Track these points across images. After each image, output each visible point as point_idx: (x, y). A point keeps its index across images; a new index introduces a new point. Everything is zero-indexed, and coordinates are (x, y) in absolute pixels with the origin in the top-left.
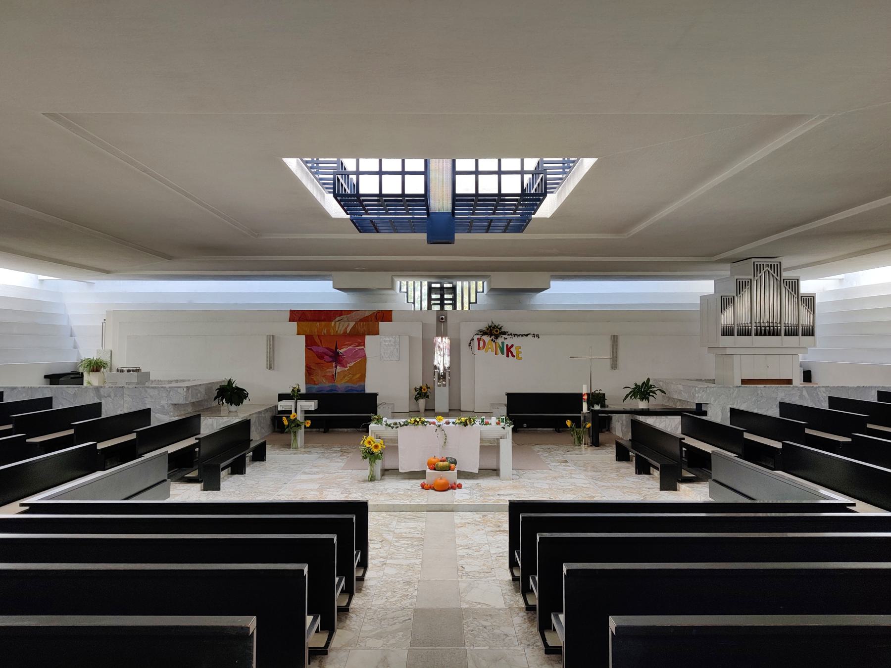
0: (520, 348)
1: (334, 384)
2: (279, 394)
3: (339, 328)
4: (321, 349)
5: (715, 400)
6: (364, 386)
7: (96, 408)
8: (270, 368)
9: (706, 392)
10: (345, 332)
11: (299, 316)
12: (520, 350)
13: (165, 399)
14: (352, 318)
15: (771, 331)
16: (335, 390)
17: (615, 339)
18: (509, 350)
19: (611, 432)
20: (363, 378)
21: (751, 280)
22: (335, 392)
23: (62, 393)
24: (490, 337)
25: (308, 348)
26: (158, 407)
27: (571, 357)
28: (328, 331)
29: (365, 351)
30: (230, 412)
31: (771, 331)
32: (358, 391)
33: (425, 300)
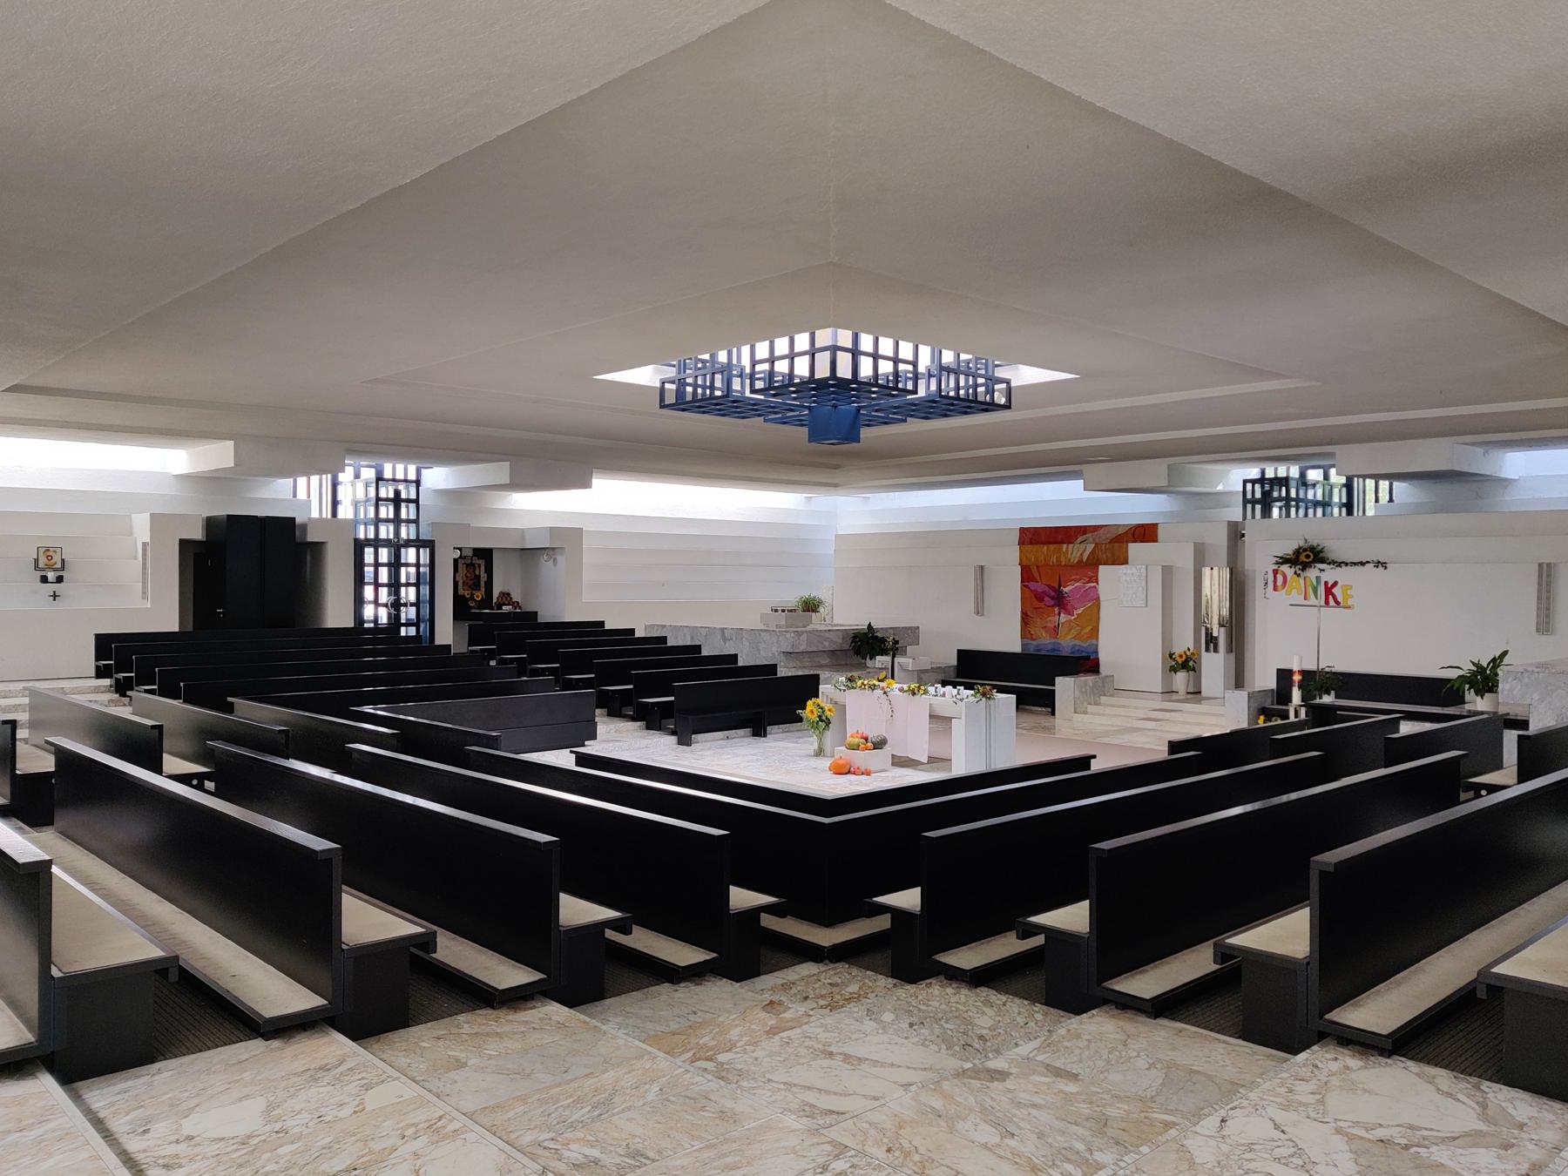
0: (1351, 587)
2: (959, 651)
3: (1071, 554)
5: (1541, 700)
6: (1097, 645)
7: (698, 648)
9: (1520, 681)
10: (1080, 561)
16: (1058, 650)
17: (1546, 573)
18: (1329, 591)
27: (1291, 605)
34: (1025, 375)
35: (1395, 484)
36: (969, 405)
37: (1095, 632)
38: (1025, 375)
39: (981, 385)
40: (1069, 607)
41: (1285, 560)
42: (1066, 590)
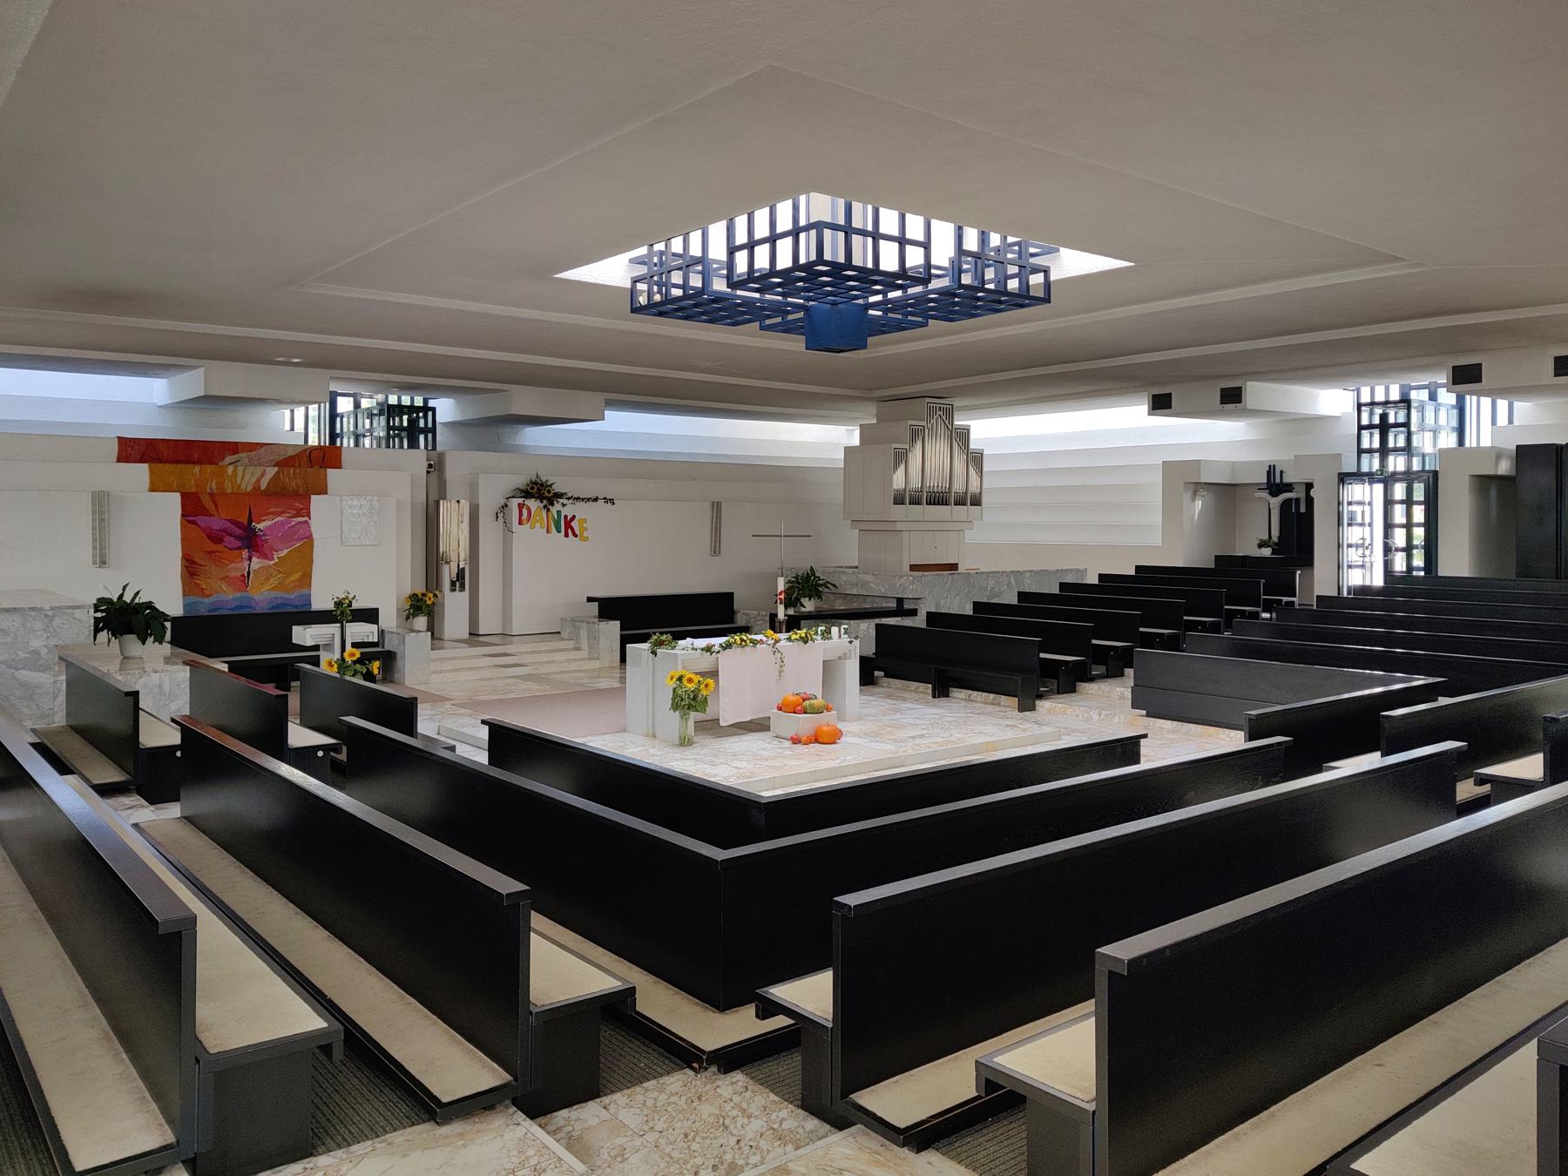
1: (245, 594)
3: (243, 478)
4: (216, 523)
8: (103, 563)
10: (257, 488)
11: (132, 450)
12: (585, 525)
13: (41, 635)
14: (259, 459)
15: (936, 500)
16: (250, 607)
17: (717, 508)
19: (399, 684)
20: (306, 579)
21: (924, 427)
22: (248, 611)
24: (542, 502)
25: (189, 521)
26: (22, 655)
28: (220, 484)
29: (309, 527)
30: (125, 658)
31: (936, 500)
32: (296, 607)
34: (1071, 263)
35: (1517, 405)
36: (1001, 301)
38: (1071, 263)
39: (1013, 276)
40: (266, 548)
41: (527, 493)
42: (261, 526)
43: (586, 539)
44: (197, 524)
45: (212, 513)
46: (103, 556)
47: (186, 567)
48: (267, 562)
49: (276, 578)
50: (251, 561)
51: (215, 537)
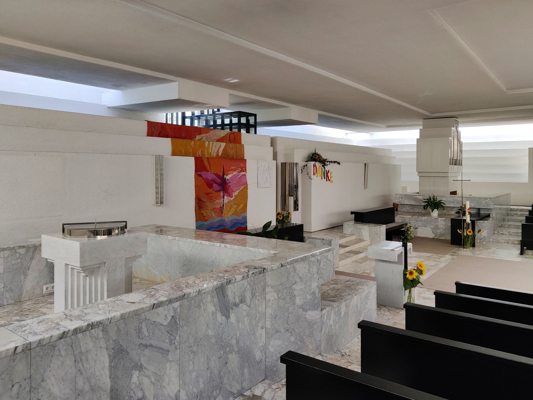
1: (221, 218)
3: (212, 149)
4: (210, 176)
10: (217, 155)
14: (210, 138)
16: (223, 226)
23: (139, 331)
33: (175, 121)
37: (245, 209)
43: (332, 182)
44: (202, 177)
45: (208, 170)
46: (162, 198)
47: (197, 203)
48: (230, 198)
49: (234, 208)
50: (224, 199)
51: (210, 185)
